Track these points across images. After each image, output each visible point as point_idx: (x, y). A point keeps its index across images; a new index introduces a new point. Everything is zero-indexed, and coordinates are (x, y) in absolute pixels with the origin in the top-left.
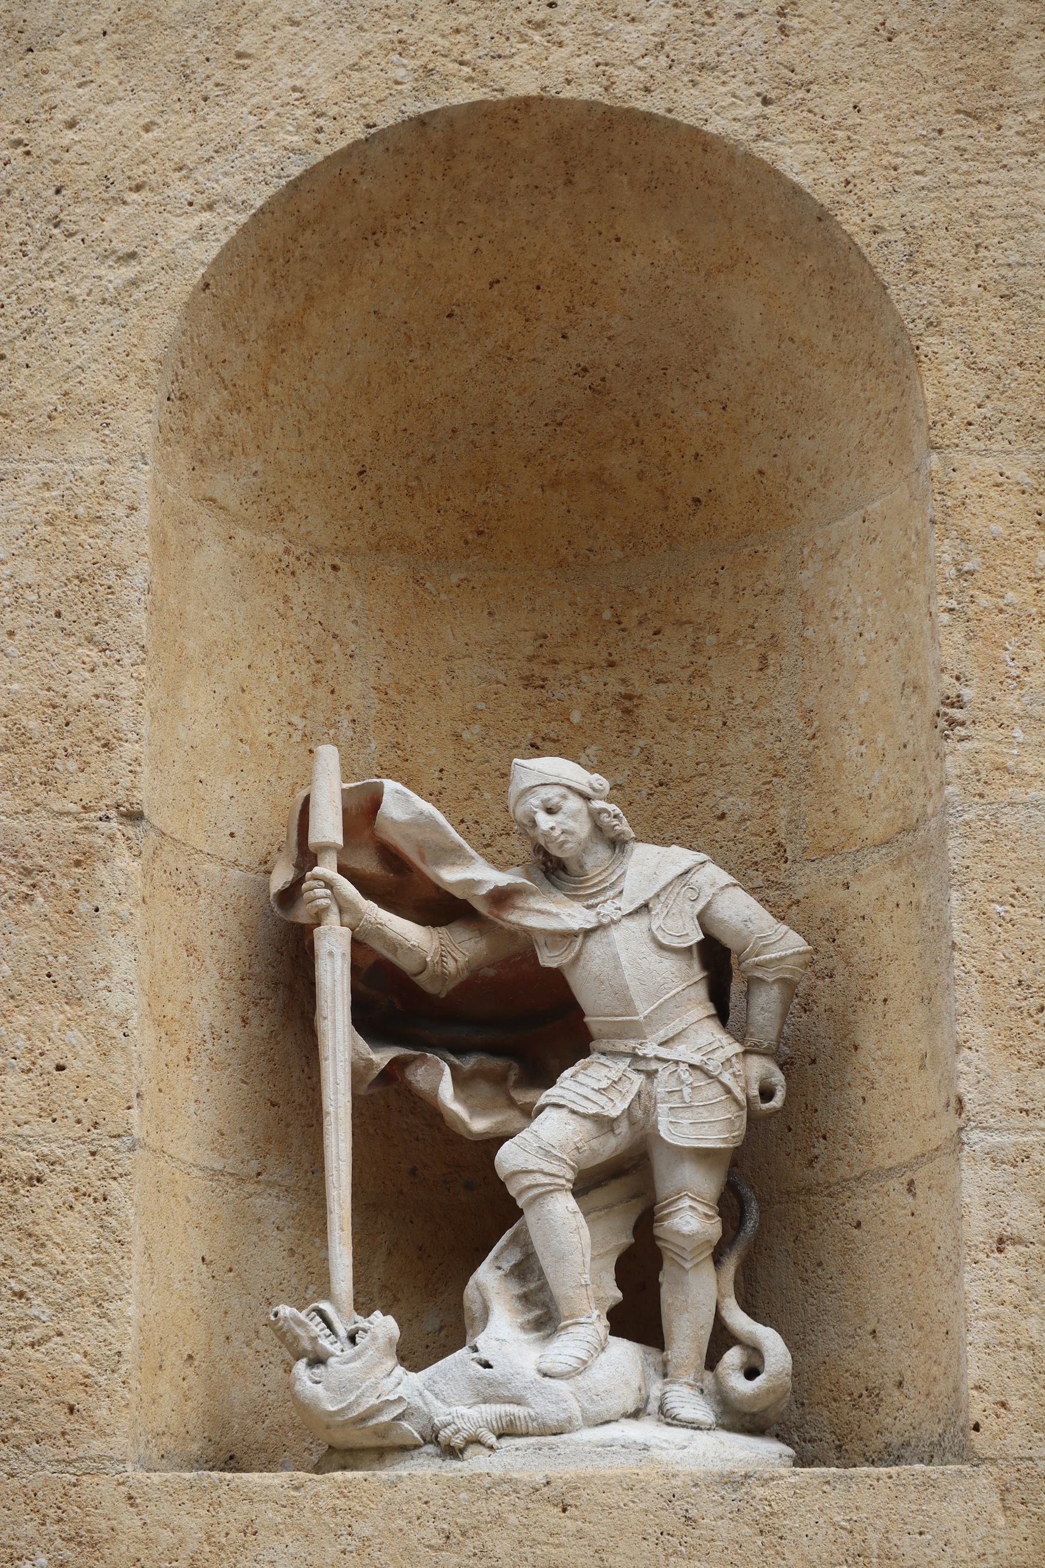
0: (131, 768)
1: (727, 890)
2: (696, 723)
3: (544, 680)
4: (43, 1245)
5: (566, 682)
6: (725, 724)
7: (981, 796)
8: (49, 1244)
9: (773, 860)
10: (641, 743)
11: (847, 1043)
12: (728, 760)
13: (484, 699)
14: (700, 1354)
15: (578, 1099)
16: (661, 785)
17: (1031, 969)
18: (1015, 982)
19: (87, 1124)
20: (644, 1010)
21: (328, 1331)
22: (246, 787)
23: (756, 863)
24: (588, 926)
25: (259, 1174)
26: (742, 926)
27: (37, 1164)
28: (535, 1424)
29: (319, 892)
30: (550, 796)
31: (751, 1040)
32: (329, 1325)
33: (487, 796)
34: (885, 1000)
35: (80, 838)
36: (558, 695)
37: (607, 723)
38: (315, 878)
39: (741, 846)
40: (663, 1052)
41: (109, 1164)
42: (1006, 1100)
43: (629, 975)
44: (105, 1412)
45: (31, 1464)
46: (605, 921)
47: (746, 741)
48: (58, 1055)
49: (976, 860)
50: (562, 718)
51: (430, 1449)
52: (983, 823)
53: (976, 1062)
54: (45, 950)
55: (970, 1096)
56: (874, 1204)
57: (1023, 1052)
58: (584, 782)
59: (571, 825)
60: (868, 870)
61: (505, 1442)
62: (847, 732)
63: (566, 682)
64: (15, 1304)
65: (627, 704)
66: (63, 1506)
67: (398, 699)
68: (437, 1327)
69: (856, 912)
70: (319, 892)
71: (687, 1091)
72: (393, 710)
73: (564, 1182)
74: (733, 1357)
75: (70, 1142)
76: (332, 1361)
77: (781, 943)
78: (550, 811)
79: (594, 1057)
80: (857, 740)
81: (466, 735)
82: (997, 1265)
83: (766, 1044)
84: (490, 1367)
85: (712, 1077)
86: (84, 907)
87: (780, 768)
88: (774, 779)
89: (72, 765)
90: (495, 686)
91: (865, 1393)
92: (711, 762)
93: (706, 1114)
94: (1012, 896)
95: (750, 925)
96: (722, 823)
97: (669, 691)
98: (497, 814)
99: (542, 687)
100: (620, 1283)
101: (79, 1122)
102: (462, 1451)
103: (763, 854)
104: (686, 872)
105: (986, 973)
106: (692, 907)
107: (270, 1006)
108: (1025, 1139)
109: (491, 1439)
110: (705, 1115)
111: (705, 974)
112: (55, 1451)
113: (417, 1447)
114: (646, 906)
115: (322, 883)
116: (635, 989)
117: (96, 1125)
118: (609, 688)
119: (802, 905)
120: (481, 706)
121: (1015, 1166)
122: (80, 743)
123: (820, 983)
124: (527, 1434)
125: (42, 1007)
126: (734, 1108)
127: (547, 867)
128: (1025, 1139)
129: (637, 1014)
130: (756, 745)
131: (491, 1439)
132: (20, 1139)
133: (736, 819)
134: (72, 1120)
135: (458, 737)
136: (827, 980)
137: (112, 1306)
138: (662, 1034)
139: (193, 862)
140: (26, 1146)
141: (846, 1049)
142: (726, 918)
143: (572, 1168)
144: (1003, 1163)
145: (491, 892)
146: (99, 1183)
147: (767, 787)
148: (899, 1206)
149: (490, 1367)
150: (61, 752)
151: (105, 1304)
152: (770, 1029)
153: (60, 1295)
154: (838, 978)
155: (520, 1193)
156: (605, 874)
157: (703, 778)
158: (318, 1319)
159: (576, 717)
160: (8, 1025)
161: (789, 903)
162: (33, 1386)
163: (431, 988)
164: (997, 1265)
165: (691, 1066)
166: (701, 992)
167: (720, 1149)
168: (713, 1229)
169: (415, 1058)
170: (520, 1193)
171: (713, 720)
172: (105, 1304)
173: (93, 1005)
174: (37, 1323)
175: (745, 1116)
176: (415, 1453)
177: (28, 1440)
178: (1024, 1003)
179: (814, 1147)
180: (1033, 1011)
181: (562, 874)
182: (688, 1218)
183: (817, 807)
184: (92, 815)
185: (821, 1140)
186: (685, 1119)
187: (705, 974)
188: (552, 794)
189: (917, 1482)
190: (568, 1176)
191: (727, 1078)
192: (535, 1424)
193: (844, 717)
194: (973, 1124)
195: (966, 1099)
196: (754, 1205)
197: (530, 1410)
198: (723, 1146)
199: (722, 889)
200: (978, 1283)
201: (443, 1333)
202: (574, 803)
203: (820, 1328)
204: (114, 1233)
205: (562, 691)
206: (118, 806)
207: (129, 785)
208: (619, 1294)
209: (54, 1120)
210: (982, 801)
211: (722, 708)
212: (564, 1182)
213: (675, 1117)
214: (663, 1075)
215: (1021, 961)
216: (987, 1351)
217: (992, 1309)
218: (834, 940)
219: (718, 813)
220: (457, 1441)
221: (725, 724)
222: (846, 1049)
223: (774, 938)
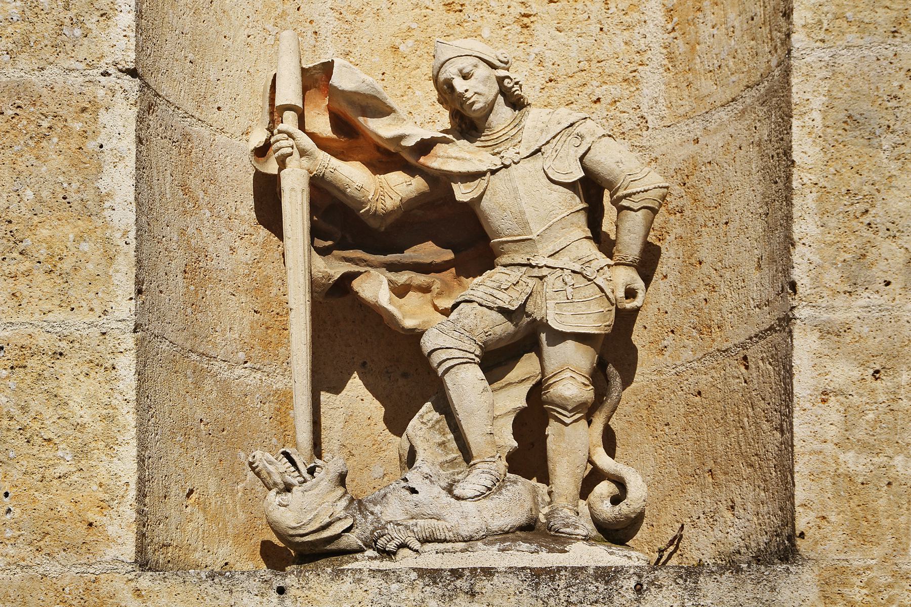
0: (125, 33)
1: (604, 139)
2: (579, 31)
3: (462, 5)
4: (66, 404)
5: (479, 7)
6: (601, 29)
7: (823, 41)
8: (71, 403)
9: (636, 130)
10: (536, 50)
11: (693, 261)
12: (602, 57)
13: (417, 21)
14: (577, 487)
15: (485, 296)
16: (551, 81)
17: (858, 180)
18: (844, 191)
19: (98, 311)
20: (536, 230)
21: (293, 469)
22: (231, 74)
23: (623, 133)
24: (494, 168)
25: (246, 362)
26: (614, 166)
27: (60, 343)
28: (451, 534)
29: (284, 143)
30: (464, 65)
31: (617, 256)
32: (293, 463)
33: (418, 93)
34: (727, 223)
35: (85, 90)
36: (472, 17)
37: (510, 36)
38: (280, 132)
39: (612, 122)
40: (551, 262)
41: (116, 342)
42: (833, 284)
43: (526, 204)
44: (116, 527)
45: (60, 567)
46: (507, 163)
47: (619, 40)
48: (74, 259)
49: (815, 94)
50: (476, 34)
51: (370, 553)
52: (823, 63)
53: (808, 255)
54: (61, 178)
55: (802, 282)
56: (712, 377)
57: (848, 246)
58: (493, 55)
59: (481, 88)
60: (714, 126)
61: (429, 547)
62: (701, 21)
63: (479, 7)
64: (45, 448)
65: (526, 20)
66: (86, 598)
67: (350, 17)
68: (382, 475)
69: (704, 159)
70: (284, 143)
71: (569, 290)
72: (347, 26)
73: (473, 356)
74: (604, 488)
75: (86, 326)
76: (294, 489)
77: (645, 179)
78: (466, 77)
79: (499, 269)
80: (710, 25)
81: (402, 48)
82: (821, 412)
83: (631, 259)
84: (417, 492)
85: (589, 280)
86: (91, 145)
87: (645, 59)
88: (640, 68)
89: (78, 32)
90: (424, 11)
91: (702, 515)
92: (589, 61)
93: (584, 308)
94: (845, 122)
95: (621, 165)
96: (597, 105)
97: (558, 8)
98: (426, 107)
99: (461, 11)
100: (516, 435)
101: (92, 310)
102: (395, 554)
103: (629, 125)
104: (572, 125)
105: (820, 185)
106: (576, 151)
107: (252, 241)
108: (848, 315)
109: (417, 545)
110: (583, 308)
111: (584, 205)
112: (79, 557)
113: (361, 550)
114: (539, 150)
115: (286, 136)
116: (530, 215)
117: (105, 312)
118: (512, 10)
119: (659, 161)
120: (414, 26)
121: (838, 336)
122: (83, 14)
123: (672, 217)
124: (445, 541)
125: (60, 222)
126: (606, 302)
127: (462, 129)
128: (848, 315)
129: (532, 233)
130: (626, 43)
131: (417, 545)
132: (45, 324)
133: (609, 101)
134: (86, 308)
135: (396, 49)
136: (678, 215)
137: (121, 449)
138: (551, 249)
139: (186, 124)
140: (50, 330)
141: (692, 264)
142: (602, 160)
143: (480, 346)
144: (828, 333)
145: (418, 144)
146: (109, 356)
147: (634, 74)
148: (733, 377)
149: (417, 492)
150: (67, 21)
151: (116, 447)
152: (634, 247)
153: (80, 441)
154: (686, 213)
155: (440, 364)
156: (507, 129)
157: (583, 73)
158: (285, 460)
159: (486, 33)
160: (32, 237)
161: (649, 160)
162: (59, 509)
163: (373, 224)
164: (821, 412)
165: (573, 272)
166: (582, 219)
167: (594, 334)
168: (588, 394)
169: (359, 274)
170: (440, 364)
171: (592, 27)
172: (116, 447)
173: (101, 221)
174: (62, 462)
175: (614, 311)
176: (359, 556)
177: (57, 550)
178: (850, 209)
179: (664, 339)
180: (858, 214)
181: (474, 132)
182: (569, 386)
183: (674, 84)
184: (95, 71)
185: (671, 334)
186: (568, 310)
187: (584, 205)
188: (466, 64)
189: (752, 577)
190: (477, 353)
191: (600, 281)
192: (451, 534)
193: (699, 10)
194: (804, 303)
195: (799, 284)
196: (618, 380)
197: (447, 524)
198: (596, 332)
199: (600, 138)
200: (805, 425)
201: (386, 479)
202: (483, 71)
203: (667, 471)
204: (121, 393)
205: (476, 13)
206: (116, 64)
207: (124, 47)
208: (516, 444)
209: (73, 309)
210: (825, 45)
211: (600, 17)
212: (473, 356)
213: (561, 310)
214: (550, 280)
215: (849, 174)
216: (812, 477)
217: (817, 446)
218: (685, 184)
219: (595, 98)
220: (391, 547)
221: (601, 29)
222: (692, 264)
223: (640, 176)
